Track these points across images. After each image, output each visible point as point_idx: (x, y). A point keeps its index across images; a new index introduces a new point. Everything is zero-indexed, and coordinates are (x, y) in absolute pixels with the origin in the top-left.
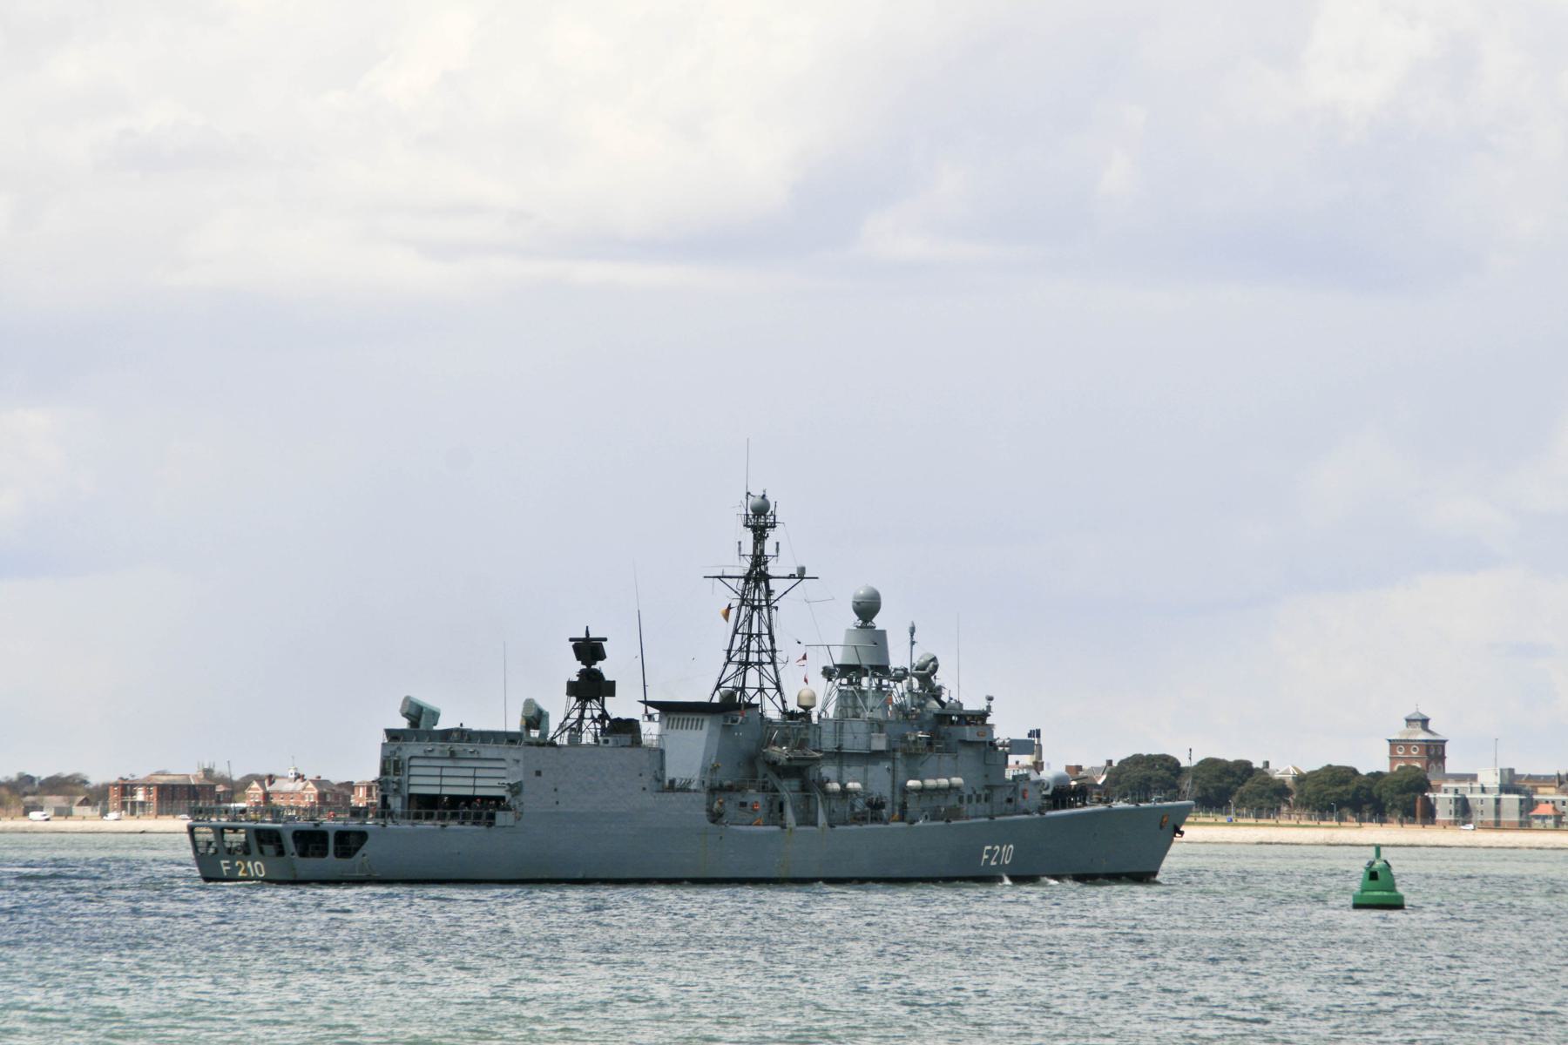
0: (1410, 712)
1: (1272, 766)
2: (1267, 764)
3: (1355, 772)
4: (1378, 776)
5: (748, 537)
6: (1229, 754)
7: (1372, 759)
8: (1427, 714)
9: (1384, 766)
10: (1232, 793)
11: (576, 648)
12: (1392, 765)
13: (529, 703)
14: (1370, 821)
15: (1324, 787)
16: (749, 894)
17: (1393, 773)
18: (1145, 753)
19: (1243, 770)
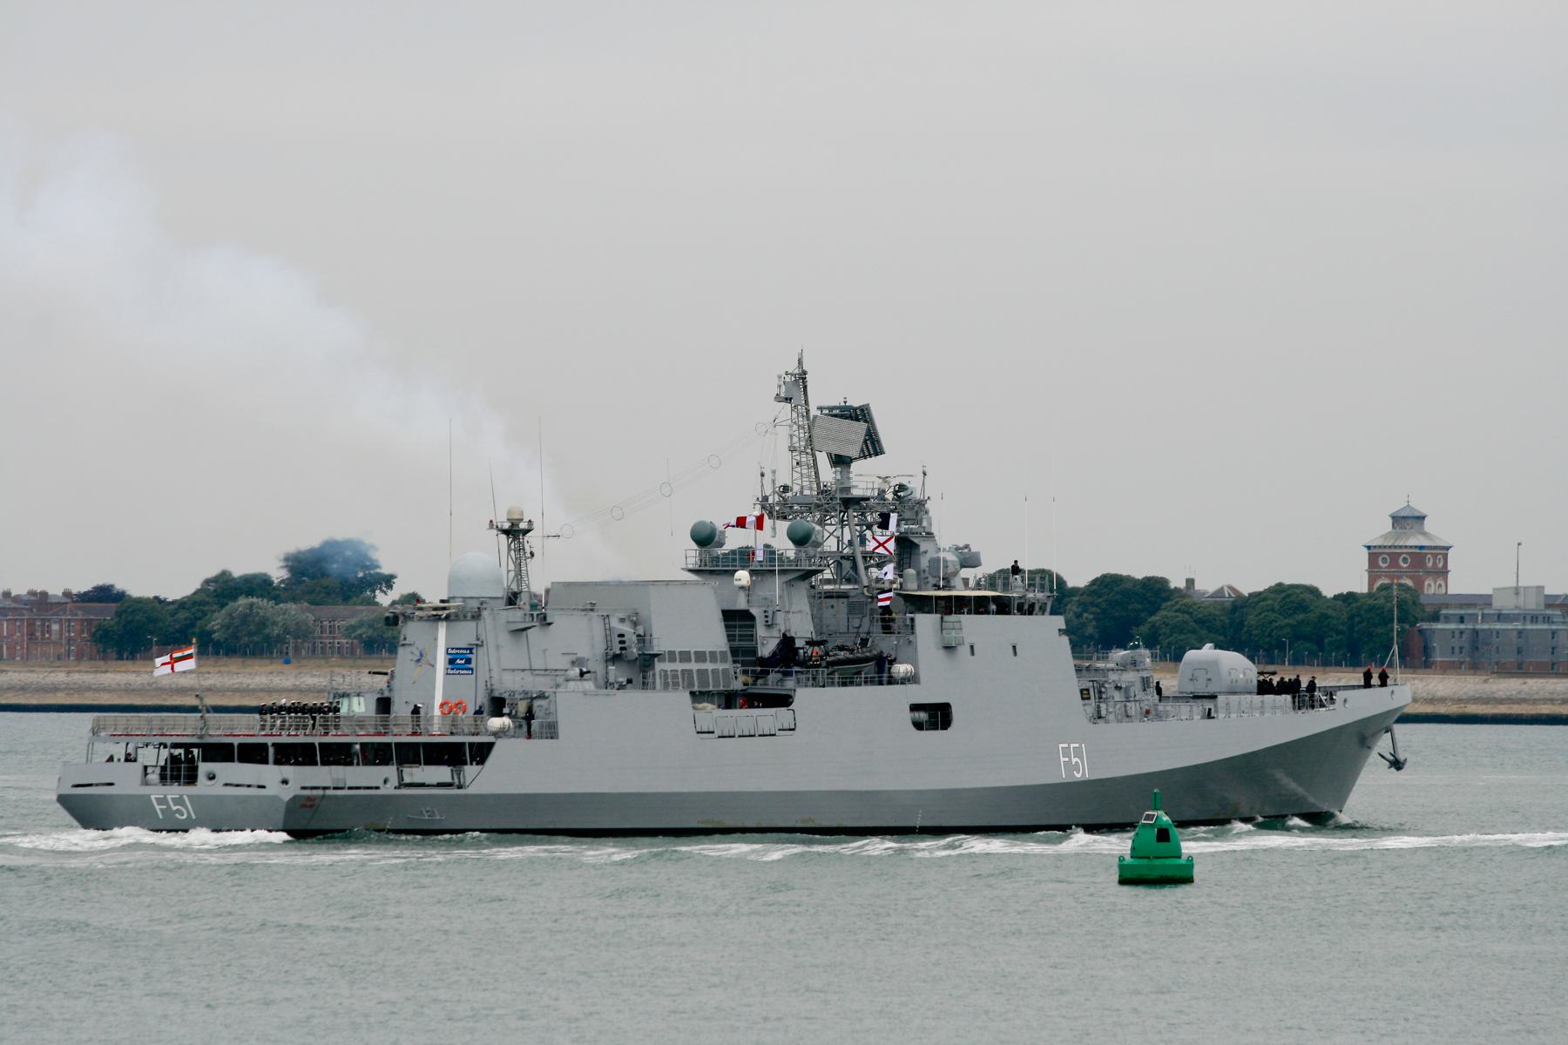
0: (1397, 506)
1: (1198, 586)
2: (1190, 582)
3: (1314, 591)
4: (1349, 598)
5: (644, 492)
6: (1137, 568)
7: (1341, 574)
8: (1421, 508)
9: (1360, 585)
10: (1138, 622)
11: (379, 700)
12: (1371, 581)
13: (551, 731)
14: (1338, 664)
15: (1272, 616)
16: (564, 849)
17: (1370, 595)
18: (1287, 582)
19: (1154, 591)
